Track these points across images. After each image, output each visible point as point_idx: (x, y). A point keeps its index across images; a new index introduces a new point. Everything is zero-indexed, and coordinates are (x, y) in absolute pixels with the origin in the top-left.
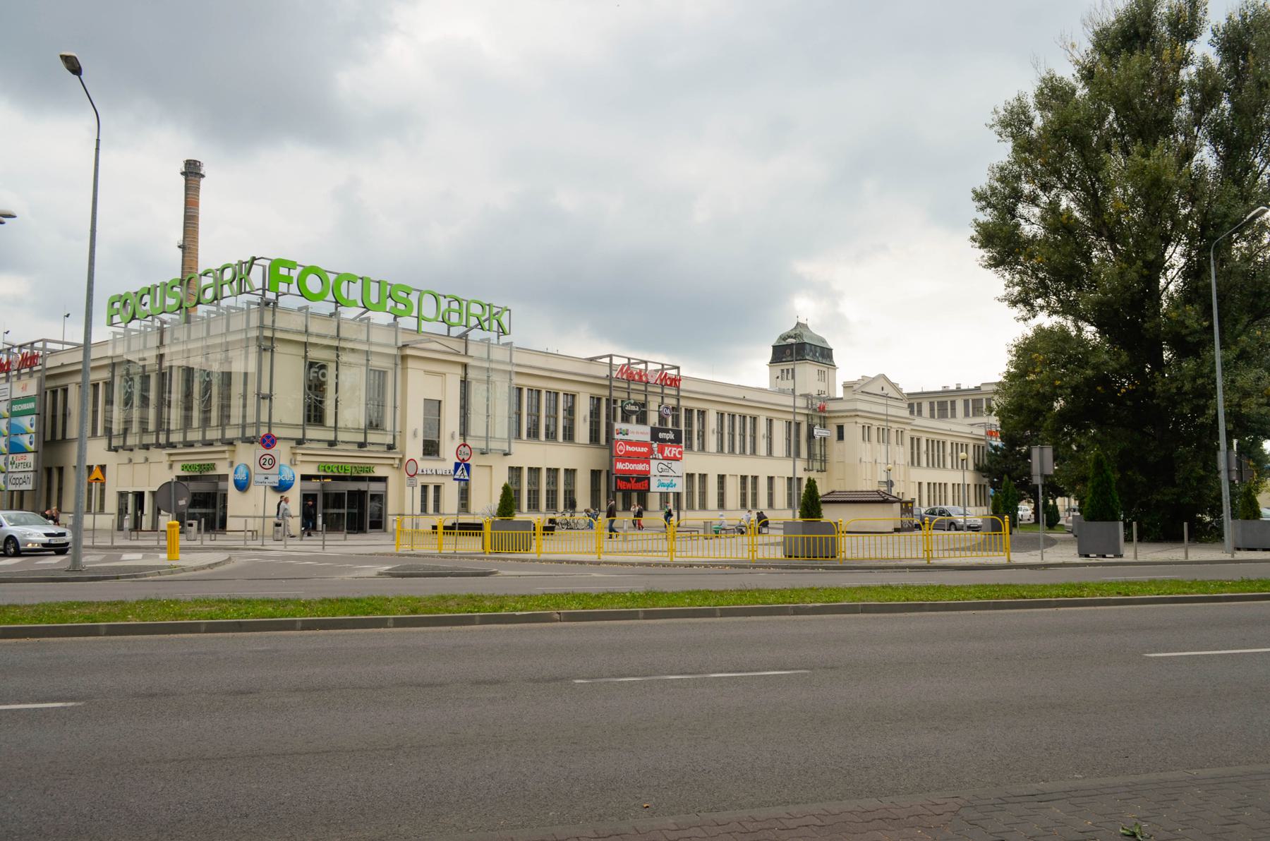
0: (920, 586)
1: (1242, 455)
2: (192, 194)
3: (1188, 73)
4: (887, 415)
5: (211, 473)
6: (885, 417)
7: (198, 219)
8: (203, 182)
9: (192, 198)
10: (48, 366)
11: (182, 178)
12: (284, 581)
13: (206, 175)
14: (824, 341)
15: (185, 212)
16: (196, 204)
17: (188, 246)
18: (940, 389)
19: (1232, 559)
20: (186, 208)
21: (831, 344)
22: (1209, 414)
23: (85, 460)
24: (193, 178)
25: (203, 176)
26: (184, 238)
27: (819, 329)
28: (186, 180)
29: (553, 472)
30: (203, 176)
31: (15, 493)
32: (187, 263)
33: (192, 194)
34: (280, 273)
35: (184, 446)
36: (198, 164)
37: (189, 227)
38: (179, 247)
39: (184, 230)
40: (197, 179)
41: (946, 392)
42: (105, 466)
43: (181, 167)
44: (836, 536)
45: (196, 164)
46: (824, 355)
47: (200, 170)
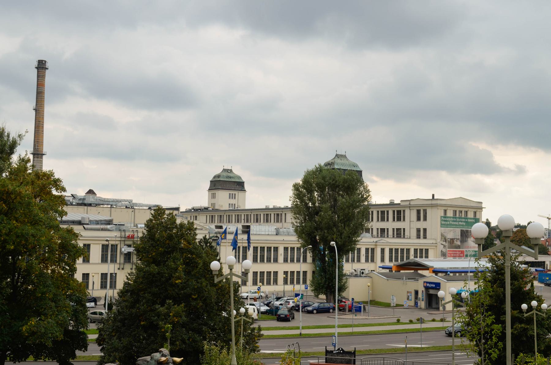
0: (454, 257)
3: (151, 298)
5: (344, 260)
7: (44, 94)
8: (47, 72)
9: (40, 90)
11: (36, 70)
13: (49, 68)
14: (240, 178)
15: (37, 90)
16: (43, 85)
17: (38, 109)
18: (264, 207)
20: (37, 88)
21: (244, 179)
23: (425, 303)
24: (41, 70)
26: (36, 105)
28: (38, 72)
29: (292, 273)
32: (37, 118)
35: (77, 237)
36: (44, 62)
37: (40, 74)
38: (34, 109)
39: (36, 100)
40: (43, 71)
41: (267, 209)
42: (426, 229)
43: (36, 64)
44: (337, 317)
45: (42, 62)
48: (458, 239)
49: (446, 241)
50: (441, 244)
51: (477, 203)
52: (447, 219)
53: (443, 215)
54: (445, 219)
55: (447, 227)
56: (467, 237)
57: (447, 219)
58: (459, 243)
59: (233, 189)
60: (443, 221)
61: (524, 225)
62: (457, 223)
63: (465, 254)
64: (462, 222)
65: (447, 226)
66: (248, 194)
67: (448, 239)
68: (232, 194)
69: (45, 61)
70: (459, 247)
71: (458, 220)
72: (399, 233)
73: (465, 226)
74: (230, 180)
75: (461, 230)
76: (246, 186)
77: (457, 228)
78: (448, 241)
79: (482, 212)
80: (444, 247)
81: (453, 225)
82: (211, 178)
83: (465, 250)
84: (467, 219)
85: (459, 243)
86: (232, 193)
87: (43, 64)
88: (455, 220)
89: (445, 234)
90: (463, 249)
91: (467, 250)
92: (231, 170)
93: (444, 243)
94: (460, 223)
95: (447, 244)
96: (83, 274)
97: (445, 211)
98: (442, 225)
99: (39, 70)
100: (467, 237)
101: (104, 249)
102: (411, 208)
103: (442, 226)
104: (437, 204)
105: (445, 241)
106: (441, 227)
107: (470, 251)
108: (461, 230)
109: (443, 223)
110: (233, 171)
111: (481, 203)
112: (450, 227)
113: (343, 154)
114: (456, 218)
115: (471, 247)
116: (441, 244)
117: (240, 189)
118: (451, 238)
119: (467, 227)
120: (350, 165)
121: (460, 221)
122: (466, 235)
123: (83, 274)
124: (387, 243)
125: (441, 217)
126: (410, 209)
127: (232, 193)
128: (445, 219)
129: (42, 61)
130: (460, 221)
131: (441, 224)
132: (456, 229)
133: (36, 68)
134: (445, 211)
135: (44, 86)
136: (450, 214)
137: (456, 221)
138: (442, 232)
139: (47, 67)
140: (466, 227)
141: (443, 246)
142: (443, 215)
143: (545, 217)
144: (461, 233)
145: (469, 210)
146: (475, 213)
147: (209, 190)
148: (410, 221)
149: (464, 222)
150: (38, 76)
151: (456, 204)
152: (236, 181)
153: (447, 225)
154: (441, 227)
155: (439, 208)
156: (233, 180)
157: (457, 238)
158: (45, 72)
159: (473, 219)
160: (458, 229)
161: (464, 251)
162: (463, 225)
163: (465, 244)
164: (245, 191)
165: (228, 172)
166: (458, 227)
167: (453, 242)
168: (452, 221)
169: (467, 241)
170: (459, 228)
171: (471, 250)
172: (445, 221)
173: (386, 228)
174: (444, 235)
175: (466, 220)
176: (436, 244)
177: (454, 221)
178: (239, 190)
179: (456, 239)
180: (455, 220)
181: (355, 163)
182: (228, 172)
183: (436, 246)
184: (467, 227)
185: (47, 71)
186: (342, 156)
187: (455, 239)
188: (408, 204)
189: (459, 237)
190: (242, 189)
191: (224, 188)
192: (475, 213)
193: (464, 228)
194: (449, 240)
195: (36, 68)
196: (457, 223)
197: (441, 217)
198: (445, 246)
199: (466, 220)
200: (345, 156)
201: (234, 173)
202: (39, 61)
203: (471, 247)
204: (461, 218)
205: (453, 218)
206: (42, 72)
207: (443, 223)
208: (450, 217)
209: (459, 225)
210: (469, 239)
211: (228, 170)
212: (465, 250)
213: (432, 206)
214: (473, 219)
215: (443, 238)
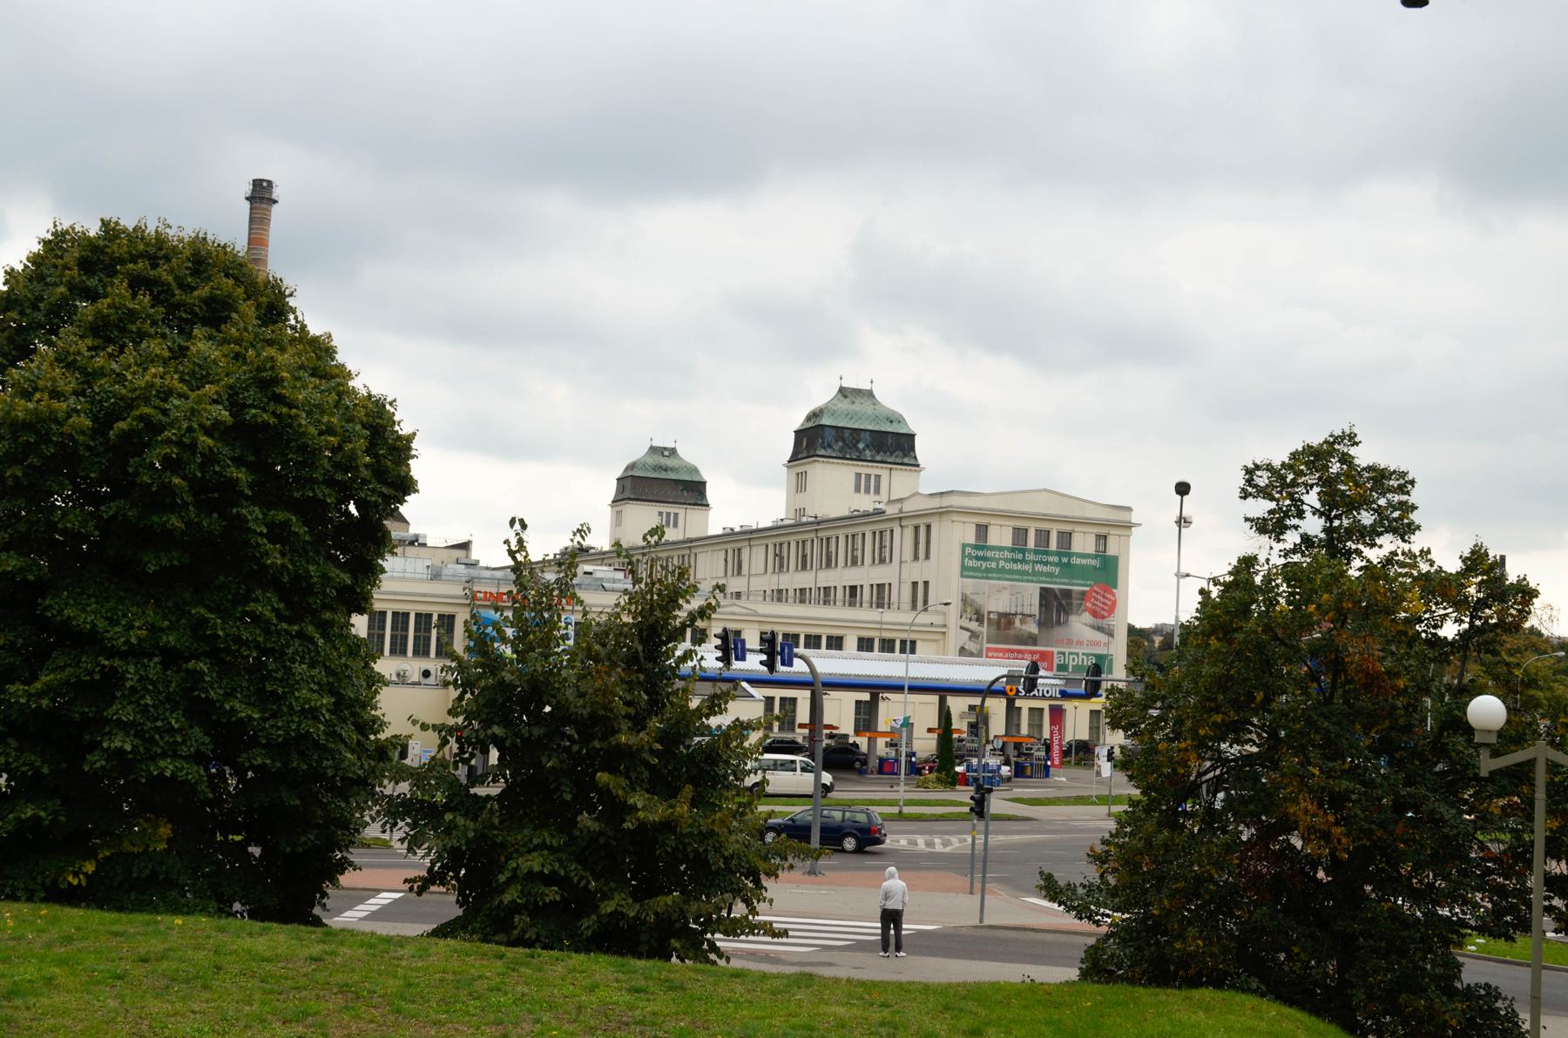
1: (395, 550)
2: (257, 229)
4: (881, 623)
6: (878, 626)
8: (275, 210)
10: (884, 620)
11: (247, 205)
12: (1508, 958)
14: (695, 470)
19: (947, 837)
21: (706, 475)
22: (11, 375)
24: (258, 205)
25: (275, 202)
27: (694, 454)
28: (251, 209)
30: (275, 202)
31: (1029, 774)
33: (257, 229)
34: (1450, 638)
40: (264, 206)
43: (247, 189)
46: (693, 491)
47: (271, 193)
48: (1030, 616)
49: (980, 620)
50: (961, 628)
51: (1108, 510)
52: (989, 554)
53: (971, 539)
54: (980, 553)
55: (988, 578)
56: (1064, 610)
57: (989, 554)
58: (1033, 628)
59: (671, 500)
60: (970, 557)
61: (415, 478)
62: (1027, 567)
63: (1056, 662)
64: (1046, 563)
65: (987, 574)
66: (712, 513)
67: (989, 613)
68: (668, 514)
69: (270, 183)
70: (1033, 640)
71: (1029, 557)
72: (881, 595)
73: (1057, 577)
74: (664, 475)
75: (1041, 588)
76: (711, 494)
77: (1028, 581)
78: (989, 619)
79: (1129, 536)
80: (970, 637)
81: (1012, 572)
82: (619, 473)
83: (1055, 650)
84: (1070, 555)
85: (1033, 628)
86: (669, 510)
87: (264, 188)
88: (1020, 556)
89: (979, 600)
90: (1047, 645)
91: (1067, 651)
92: (673, 451)
93: (974, 626)
94: (1039, 567)
95: (984, 630)
96: (857, 701)
97: (982, 530)
98: (965, 571)
99: (254, 205)
100: (1064, 610)
101: (419, 646)
102: (904, 523)
103: (966, 573)
104: (951, 507)
105: (977, 620)
106: (962, 576)
107: (1077, 654)
108: (1041, 588)
109: (971, 563)
110: (680, 452)
111: (1129, 509)
112: (999, 579)
113: (865, 386)
114: (1023, 551)
115: (1080, 643)
116: (961, 628)
117: (692, 502)
118: (1001, 611)
119: (1067, 581)
120: (876, 418)
121: (1037, 562)
122: (1060, 604)
123: (857, 701)
124: (747, 615)
125: (964, 546)
126: (902, 527)
127: (669, 510)
128: (980, 553)
129: (262, 181)
130: (1037, 562)
131: (964, 568)
132: (1024, 584)
133: (247, 199)
134: (982, 530)
135: (267, 246)
136: (1000, 536)
137: (1023, 561)
138: (968, 593)
139: (274, 196)
140: (1063, 580)
141: (969, 634)
142: (971, 538)
143: (909, 497)
144: (1042, 597)
145: (1111, 532)
146: (1102, 539)
147: (613, 502)
148: (901, 562)
149: (1056, 565)
150: (251, 220)
151: (1014, 509)
152: (681, 478)
153: (988, 570)
154: (962, 576)
155: (955, 517)
156: (672, 476)
157: (1027, 611)
158: (270, 211)
159: (1096, 557)
160: (1031, 584)
161: (1053, 653)
162: (1050, 575)
163: (1058, 632)
164: (708, 505)
165: (664, 456)
166: (1030, 578)
167: (1010, 623)
168: (1007, 560)
169: (1066, 622)
170: (1032, 581)
171: (1080, 651)
172: (978, 558)
173: (831, 584)
174: (973, 601)
175: (1065, 560)
176: (945, 626)
177: (1015, 561)
178: (690, 504)
179: (1023, 614)
180: (1020, 556)
181: (894, 412)
182: (663, 454)
183: (944, 633)
184: (1067, 581)
185: (275, 208)
186: (858, 392)
187: (1016, 614)
188: (897, 511)
189: (1035, 610)
190: (699, 502)
191: (650, 498)
192: (1102, 539)
193: (1055, 583)
194: (992, 616)
195: (247, 199)
196: (1027, 567)
197: (964, 546)
198: (974, 635)
199: (1065, 560)
200: (869, 394)
201: (681, 458)
202: (254, 181)
203: (1080, 643)
204: (1047, 553)
205: (1012, 550)
206: (259, 209)
207: (971, 563)
208: (1001, 549)
209: (1035, 573)
210: (1073, 618)
211: (665, 449)
212: (1055, 650)
213: (942, 513)
214: (1096, 557)
215: (969, 609)
